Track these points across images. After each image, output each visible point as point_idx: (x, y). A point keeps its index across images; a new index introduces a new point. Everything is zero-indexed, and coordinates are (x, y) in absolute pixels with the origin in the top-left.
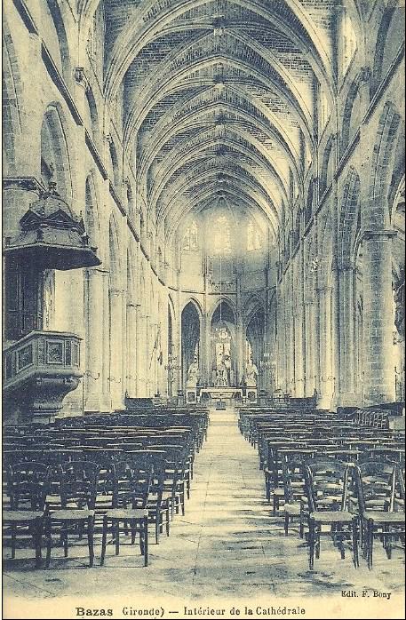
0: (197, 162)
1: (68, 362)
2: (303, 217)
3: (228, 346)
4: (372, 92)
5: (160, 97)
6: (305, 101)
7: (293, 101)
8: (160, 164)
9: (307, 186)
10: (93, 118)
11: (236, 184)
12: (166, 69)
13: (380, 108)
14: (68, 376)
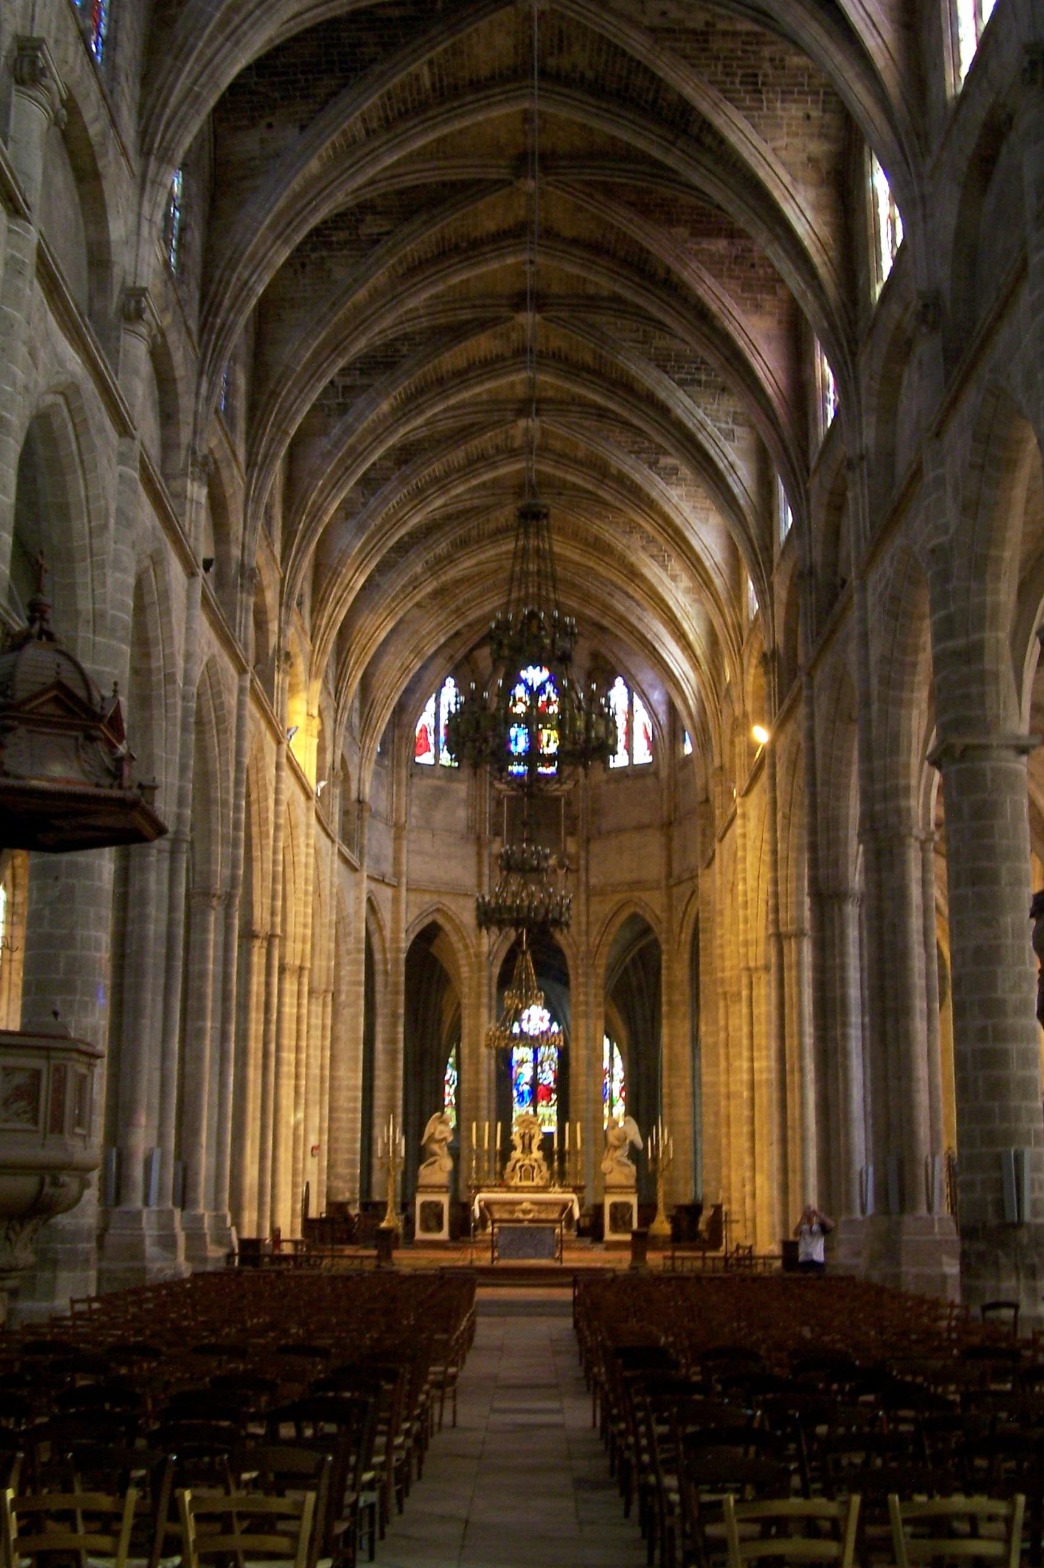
1: (57, 1126)
3: (548, 1053)
4: (951, 356)
5: (359, 346)
10: (167, 416)
12: (380, 278)
13: (971, 398)
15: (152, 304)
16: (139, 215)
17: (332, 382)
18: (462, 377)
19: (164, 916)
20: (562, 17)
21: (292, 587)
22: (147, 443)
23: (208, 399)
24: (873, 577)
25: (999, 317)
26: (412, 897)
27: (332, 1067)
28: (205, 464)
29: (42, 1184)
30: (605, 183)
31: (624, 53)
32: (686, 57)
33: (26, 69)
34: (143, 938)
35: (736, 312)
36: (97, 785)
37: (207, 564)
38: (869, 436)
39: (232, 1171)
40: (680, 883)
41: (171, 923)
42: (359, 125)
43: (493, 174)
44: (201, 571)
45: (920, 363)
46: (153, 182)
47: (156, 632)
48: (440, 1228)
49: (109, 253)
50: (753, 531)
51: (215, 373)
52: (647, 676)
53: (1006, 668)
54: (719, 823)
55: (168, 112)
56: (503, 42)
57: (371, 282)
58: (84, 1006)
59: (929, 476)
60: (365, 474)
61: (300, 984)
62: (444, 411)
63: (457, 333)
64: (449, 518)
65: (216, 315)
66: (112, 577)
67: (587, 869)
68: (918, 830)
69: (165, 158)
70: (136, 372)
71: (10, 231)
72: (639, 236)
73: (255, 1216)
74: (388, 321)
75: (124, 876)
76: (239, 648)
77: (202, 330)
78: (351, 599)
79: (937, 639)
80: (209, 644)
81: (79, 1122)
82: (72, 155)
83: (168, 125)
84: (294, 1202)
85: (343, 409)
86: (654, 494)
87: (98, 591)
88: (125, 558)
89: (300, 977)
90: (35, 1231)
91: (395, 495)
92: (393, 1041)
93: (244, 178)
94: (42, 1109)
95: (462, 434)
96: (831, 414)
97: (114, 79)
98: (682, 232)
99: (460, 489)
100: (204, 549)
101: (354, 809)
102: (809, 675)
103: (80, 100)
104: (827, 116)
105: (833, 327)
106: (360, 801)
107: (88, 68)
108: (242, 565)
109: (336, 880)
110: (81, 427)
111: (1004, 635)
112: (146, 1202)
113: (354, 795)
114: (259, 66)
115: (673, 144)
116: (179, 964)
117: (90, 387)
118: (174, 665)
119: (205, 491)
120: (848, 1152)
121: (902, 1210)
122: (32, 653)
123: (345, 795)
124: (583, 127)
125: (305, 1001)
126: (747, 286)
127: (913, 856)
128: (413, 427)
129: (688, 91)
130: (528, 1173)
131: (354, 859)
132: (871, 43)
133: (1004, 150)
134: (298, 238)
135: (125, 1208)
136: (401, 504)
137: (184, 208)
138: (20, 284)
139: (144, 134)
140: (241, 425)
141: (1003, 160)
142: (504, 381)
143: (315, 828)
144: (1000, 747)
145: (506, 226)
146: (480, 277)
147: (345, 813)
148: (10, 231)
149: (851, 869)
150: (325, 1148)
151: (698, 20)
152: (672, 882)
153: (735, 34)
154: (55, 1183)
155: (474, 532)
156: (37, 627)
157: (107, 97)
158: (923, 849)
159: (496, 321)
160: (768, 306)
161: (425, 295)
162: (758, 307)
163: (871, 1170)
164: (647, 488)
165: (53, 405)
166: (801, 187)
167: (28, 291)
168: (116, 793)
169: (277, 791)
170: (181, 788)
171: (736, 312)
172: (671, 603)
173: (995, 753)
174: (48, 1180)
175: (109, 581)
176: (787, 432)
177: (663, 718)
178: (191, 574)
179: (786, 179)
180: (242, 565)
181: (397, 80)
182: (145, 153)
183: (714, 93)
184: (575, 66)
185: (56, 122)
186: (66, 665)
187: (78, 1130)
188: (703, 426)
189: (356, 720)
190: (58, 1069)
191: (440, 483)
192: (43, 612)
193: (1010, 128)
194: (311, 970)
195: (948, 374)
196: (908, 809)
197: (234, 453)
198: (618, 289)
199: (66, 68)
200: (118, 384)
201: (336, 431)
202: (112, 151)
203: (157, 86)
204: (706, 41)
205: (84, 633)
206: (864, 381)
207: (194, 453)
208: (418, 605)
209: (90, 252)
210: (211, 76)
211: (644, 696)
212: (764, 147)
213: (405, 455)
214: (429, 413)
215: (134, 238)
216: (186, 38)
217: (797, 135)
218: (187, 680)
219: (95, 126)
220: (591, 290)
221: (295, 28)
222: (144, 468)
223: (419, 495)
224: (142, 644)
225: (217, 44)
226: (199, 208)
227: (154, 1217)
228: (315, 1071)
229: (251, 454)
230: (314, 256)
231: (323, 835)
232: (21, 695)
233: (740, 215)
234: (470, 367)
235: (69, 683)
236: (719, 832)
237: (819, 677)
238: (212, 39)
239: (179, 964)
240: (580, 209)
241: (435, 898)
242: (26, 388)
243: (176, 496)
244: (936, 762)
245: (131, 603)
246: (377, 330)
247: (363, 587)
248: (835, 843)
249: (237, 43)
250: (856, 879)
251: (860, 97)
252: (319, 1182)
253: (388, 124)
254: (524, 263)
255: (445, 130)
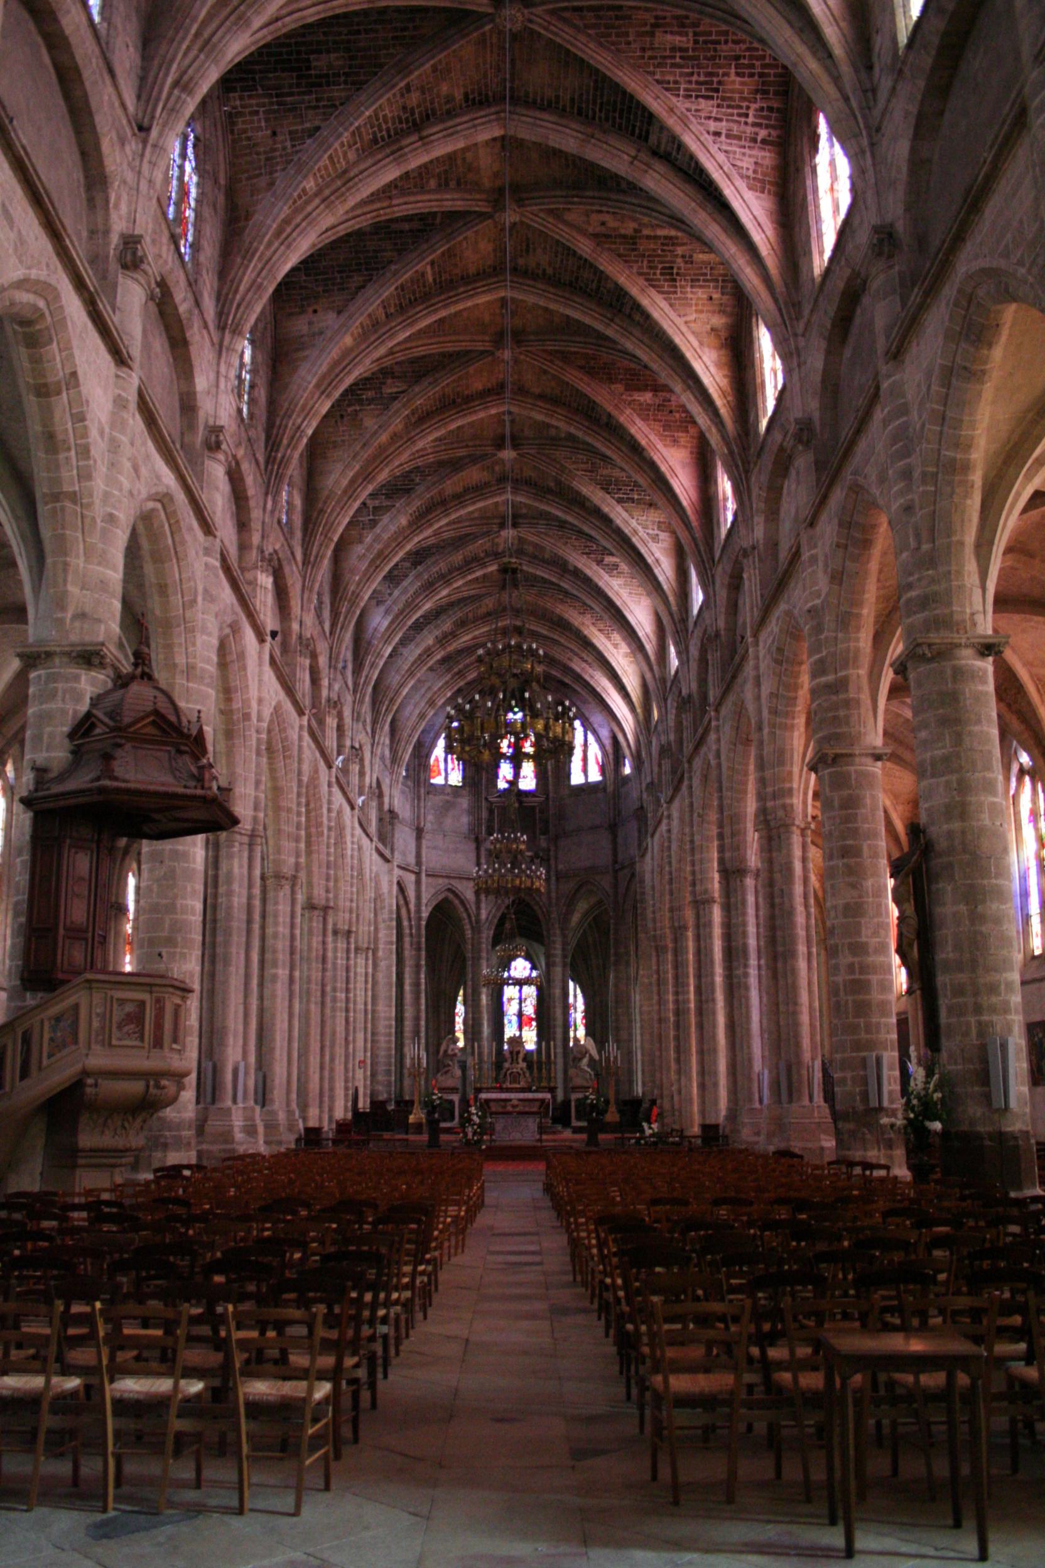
0: (462, 601)
1: (158, 1043)
2: (687, 719)
3: (530, 991)
4: (820, 466)
5: (383, 476)
6: (683, 484)
7: (661, 483)
8: (382, 609)
9: (694, 652)
10: (242, 525)
11: (556, 652)
13: (838, 496)
14: (158, 1075)
15: (228, 440)
16: (218, 373)
17: (364, 504)
18: (460, 498)
19: (245, 892)
20: (529, 227)
21: (339, 654)
22: (227, 542)
23: (273, 512)
24: (763, 636)
25: (858, 431)
26: (430, 880)
27: (374, 1003)
28: (270, 561)
29: (148, 1086)
30: (562, 352)
31: (575, 252)
32: (620, 256)
33: (129, 257)
34: (230, 907)
35: (660, 446)
36: (185, 787)
37: (274, 634)
38: (759, 532)
39: (299, 1079)
40: (623, 868)
41: (250, 897)
42: (381, 310)
43: (480, 347)
44: (269, 638)
45: (798, 473)
46: (228, 349)
47: (235, 682)
48: (452, 1118)
49: (195, 400)
50: (674, 608)
51: (277, 493)
52: (597, 718)
53: (865, 697)
54: (651, 823)
55: (238, 297)
56: (486, 247)
57: (391, 429)
58: (184, 956)
59: (806, 556)
60: (390, 572)
61: (348, 943)
62: (447, 524)
63: (455, 465)
64: (451, 605)
65: (277, 451)
66: (201, 639)
67: (556, 858)
68: (799, 821)
69: (237, 331)
70: (217, 489)
71: (117, 376)
72: (587, 390)
73: (317, 1111)
74: (405, 457)
75: (214, 862)
76: (299, 696)
77: (267, 463)
78: (381, 663)
79: (814, 676)
80: (277, 693)
81: (175, 1040)
82: (167, 328)
83: (239, 306)
84: (346, 1101)
85: (374, 523)
86: (601, 584)
87: (191, 649)
88: (209, 625)
89: (348, 938)
90: (144, 1121)
91: (410, 584)
92: (417, 984)
93: (298, 350)
94: (147, 1027)
95: (459, 542)
96: (730, 518)
97: (198, 272)
98: (619, 388)
99: (460, 583)
100: (269, 620)
101: (387, 817)
102: (717, 711)
103: (171, 284)
104: (726, 297)
105: (731, 453)
106: (391, 811)
107: (177, 262)
108: (300, 637)
109: (374, 868)
110: (175, 528)
111: (863, 672)
112: (235, 1101)
113: (386, 807)
114: (307, 265)
115: (612, 320)
116: (256, 927)
117: (181, 497)
118: (249, 707)
119: (270, 580)
120: (750, 1060)
121: (790, 1101)
122: (135, 688)
123: (381, 805)
124: (546, 309)
125: (352, 955)
126: (667, 427)
127: (796, 839)
128: (424, 536)
129: (622, 280)
130: (515, 1078)
131: (387, 853)
132: (757, 237)
133: (859, 311)
134: (337, 394)
135: (219, 1105)
136: (416, 594)
137: (254, 372)
138: (125, 415)
139: (221, 314)
140: (298, 534)
141: (858, 320)
142: (490, 501)
143: (358, 831)
144: (861, 755)
145: (489, 385)
146: (471, 425)
147: (380, 820)
148: (117, 376)
149: (749, 852)
150: (369, 1061)
151: (629, 228)
152: (617, 867)
153: (656, 237)
154: (158, 1086)
155: (471, 615)
156: (139, 670)
157: (192, 284)
158: (803, 835)
159: (484, 457)
160: (682, 441)
161: (431, 438)
162: (675, 442)
163: (766, 1072)
164: (596, 580)
165: (153, 510)
166: (706, 350)
167: (131, 421)
168: (199, 792)
169: (329, 802)
170: (256, 797)
171: (660, 446)
172: (614, 664)
173: (857, 760)
174: (152, 1083)
175: (199, 643)
176: (698, 534)
177: (609, 748)
178: (262, 641)
179: (696, 344)
180: (300, 637)
181: (407, 276)
182: (222, 328)
183: (641, 281)
184: (538, 265)
185: (151, 297)
186: (161, 698)
187: (175, 1046)
188: (636, 532)
189: (387, 752)
190: (158, 1001)
191: (445, 578)
192: (144, 659)
193: (864, 290)
194: (357, 932)
195: (818, 480)
196: (792, 805)
197: (293, 553)
198: (572, 430)
199: (161, 262)
200: (204, 497)
201: (368, 539)
202: (197, 324)
203: (230, 277)
204: (635, 244)
205: (180, 680)
206: (755, 491)
207: (262, 552)
208: (431, 669)
209: (181, 400)
210: (270, 271)
211: (595, 733)
212: (679, 321)
213: (418, 557)
214: (436, 526)
215: (214, 390)
216: (251, 243)
217: (702, 312)
218: (260, 719)
219: (184, 306)
220: (553, 432)
221: (331, 236)
222: (224, 559)
223: (429, 587)
224: (227, 692)
225: (273, 249)
226: (263, 372)
227: (240, 1112)
228: (361, 1007)
229: (306, 555)
230: (350, 410)
231: (363, 836)
232: (127, 720)
233: (664, 374)
234: (467, 490)
235: (163, 711)
236: (650, 830)
237: (724, 711)
238: (270, 244)
239: (256, 927)
240: (545, 372)
241: (447, 881)
242: (131, 493)
243: (250, 583)
244: (813, 768)
245: (215, 659)
246: (397, 463)
247: (391, 656)
248: (738, 833)
249: (288, 247)
250: (753, 859)
251: (750, 277)
252: (365, 1087)
253: (402, 309)
254: (503, 413)
255: (443, 313)
